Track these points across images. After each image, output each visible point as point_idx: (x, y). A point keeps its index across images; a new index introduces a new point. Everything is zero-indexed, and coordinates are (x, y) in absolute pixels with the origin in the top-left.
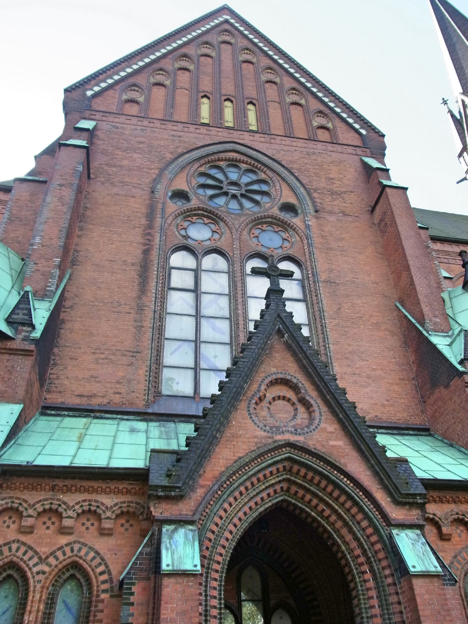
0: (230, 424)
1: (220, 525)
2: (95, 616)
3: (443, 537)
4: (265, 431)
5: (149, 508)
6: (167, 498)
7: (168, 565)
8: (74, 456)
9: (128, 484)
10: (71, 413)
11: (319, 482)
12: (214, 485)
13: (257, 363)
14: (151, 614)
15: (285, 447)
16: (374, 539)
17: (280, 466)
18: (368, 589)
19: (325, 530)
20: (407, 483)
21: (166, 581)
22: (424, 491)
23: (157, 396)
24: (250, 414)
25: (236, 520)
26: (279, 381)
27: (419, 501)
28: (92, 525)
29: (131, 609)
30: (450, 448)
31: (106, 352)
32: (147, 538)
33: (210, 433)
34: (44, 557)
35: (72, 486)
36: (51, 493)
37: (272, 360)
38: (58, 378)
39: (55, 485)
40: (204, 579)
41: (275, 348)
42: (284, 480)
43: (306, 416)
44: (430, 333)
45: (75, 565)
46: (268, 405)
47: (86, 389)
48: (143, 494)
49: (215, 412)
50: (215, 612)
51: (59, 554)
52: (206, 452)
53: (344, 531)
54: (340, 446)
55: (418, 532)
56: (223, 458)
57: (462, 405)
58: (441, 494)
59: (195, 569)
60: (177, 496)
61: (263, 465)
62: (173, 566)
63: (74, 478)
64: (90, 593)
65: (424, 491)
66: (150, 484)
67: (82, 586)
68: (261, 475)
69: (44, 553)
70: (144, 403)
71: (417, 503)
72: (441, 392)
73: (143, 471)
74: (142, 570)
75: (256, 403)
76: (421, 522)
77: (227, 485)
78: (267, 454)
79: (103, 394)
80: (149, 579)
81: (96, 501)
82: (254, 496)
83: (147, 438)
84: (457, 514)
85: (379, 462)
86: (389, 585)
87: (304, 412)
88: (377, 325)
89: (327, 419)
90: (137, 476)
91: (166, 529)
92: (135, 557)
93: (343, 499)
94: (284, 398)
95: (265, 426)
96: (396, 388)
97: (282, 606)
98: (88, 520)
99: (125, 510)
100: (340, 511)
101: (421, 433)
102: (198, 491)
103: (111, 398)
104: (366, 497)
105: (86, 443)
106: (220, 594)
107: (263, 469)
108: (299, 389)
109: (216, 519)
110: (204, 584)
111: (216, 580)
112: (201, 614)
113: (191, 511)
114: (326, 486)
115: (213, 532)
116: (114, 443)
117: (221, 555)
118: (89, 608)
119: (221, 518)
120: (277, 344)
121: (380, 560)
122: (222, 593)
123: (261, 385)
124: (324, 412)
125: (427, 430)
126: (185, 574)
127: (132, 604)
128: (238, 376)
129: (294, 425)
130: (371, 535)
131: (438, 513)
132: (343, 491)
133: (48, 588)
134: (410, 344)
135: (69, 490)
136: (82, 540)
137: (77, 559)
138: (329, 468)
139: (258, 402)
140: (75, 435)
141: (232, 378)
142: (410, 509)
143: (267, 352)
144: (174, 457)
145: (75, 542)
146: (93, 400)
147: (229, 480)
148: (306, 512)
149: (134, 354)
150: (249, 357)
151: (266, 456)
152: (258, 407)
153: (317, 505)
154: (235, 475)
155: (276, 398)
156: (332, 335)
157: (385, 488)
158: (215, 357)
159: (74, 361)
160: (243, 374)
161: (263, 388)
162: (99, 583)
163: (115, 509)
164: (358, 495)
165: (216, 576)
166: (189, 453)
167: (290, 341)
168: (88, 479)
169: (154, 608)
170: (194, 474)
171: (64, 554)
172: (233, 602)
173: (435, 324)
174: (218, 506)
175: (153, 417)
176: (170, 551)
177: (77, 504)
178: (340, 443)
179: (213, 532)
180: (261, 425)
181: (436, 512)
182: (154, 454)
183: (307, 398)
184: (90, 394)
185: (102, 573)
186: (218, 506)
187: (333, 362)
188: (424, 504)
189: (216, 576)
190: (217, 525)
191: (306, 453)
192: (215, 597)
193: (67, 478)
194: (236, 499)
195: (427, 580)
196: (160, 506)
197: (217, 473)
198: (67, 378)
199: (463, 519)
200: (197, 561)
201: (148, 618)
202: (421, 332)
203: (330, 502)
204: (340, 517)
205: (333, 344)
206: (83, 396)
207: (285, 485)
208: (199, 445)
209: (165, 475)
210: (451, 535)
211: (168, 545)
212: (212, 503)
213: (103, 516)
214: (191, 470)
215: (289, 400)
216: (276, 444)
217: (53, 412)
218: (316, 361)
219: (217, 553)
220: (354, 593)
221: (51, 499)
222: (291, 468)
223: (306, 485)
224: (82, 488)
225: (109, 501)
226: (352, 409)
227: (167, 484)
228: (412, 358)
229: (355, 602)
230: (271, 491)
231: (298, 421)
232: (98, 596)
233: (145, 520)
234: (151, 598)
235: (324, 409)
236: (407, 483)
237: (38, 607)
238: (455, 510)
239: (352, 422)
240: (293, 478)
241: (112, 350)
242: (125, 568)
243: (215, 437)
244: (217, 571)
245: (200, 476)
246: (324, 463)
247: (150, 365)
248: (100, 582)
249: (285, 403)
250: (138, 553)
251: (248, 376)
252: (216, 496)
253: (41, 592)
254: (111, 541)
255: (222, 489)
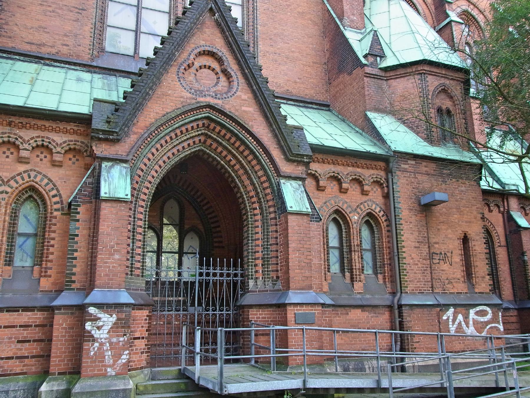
0: (161, 84)
1: (148, 165)
2: (50, 228)
3: (319, 188)
4: (190, 93)
5: (91, 147)
6: (106, 140)
7: (106, 193)
8: (28, 97)
9: (75, 126)
10: (22, 58)
11: (230, 138)
12: (145, 133)
13: (189, 35)
14: (92, 228)
15: (205, 108)
16: (266, 185)
17: (200, 123)
18: (256, 221)
19: (230, 175)
20: (299, 146)
21: (104, 205)
22: (311, 153)
23: (101, 52)
24: (179, 78)
25: (161, 162)
26: (207, 53)
27: (306, 160)
28: (45, 157)
29: (77, 224)
30: (342, 122)
31: (54, 6)
32: (90, 171)
33: (143, 90)
34: (6, 180)
35: (26, 123)
36: (8, 128)
37: (202, 35)
38: (7, 24)
39: (11, 121)
40: (133, 205)
41: (206, 24)
42: (202, 134)
43: (226, 84)
44: (346, 28)
45: (32, 188)
46: (195, 72)
47: (35, 38)
48: (87, 135)
49: (149, 73)
50: (140, 230)
51: (18, 178)
52: (140, 105)
53: (244, 178)
54: (250, 112)
55: (300, 183)
56: (154, 112)
57: (358, 90)
58: (324, 157)
59: (126, 197)
60: (114, 139)
61: (187, 121)
62: (110, 194)
63: (27, 117)
64: (45, 211)
65: (311, 153)
66: (92, 127)
67: (38, 205)
68: (184, 129)
69: (6, 177)
70: (89, 56)
71: (304, 162)
72: (345, 78)
73: (87, 116)
74: (85, 195)
75: (185, 69)
76: (304, 176)
77: (156, 134)
78: (190, 112)
79: (52, 45)
80: (91, 202)
81: (48, 138)
82: (177, 145)
83: (92, 88)
84: (334, 172)
85: (280, 128)
86: (271, 219)
87: (224, 81)
88: (302, 14)
89: (242, 89)
90: (83, 121)
91: (104, 164)
92: (80, 185)
93: (246, 153)
94: (209, 67)
95: (191, 89)
96: (309, 69)
97: (193, 229)
98: (42, 153)
99: (72, 147)
100: (243, 162)
101: (322, 108)
102: (132, 136)
103: (60, 49)
104: (265, 153)
105: (37, 87)
106: (146, 217)
107: (186, 124)
108: (223, 62)
109: (146, 160)
110: (133, 209)
111: (142, 207)
112: (129, 231)
113: (125, 152)
114: (235, 142)
115: (142, 170)
116: (62, 89)
117: (148, 188)
118: (45, 221)
119: (149, 160)
120: (208, 20)
121: (268, 201)
122: (147, 216)
123: (191, 54)
124: (241, 83)
125: (328, 106)
126: (118, 201)
127: (78, 221)
128: (171, 44)
129: (215, 91)
130: (264, 182)
131: (319, 171)
132: (247, 147)
133: (11, 205)
134: (328, 34)
135: (23, 126)
136: (37, 169)
137: (35, 184)
138: (239, 128)
139: (187, 68)
140: (27, 78)
141: (165, 46)
142: (297, 165)
143: (199, 26)
144: (113, 107)
145: (31, 170)
146: (43, 48)
147: (157, 130)
148: (217, 161)
149: (80, 11)
150: (182, 29)
151: (189, 114)
152: (187, 73)
153: (226, 156)
154: (162, 126)
155: (203, 67)
156: (261, 18)
157: (281, 148)
158: (155, 23)
159: (22, 9)
160: (176, 43)
161: (192, 57)
162: (53, 204)
163: (64, 145)
164: (258, 152)
165: (143, 204)
166: (125, 105)
167: (219, 20)
168: (40, 119)
169: (94, 224)
170: (128, 123)
171: (23, 179)
172: (156, 225)
173: (352, 21)
174: (147, 150)
175: (97, 70)
176: (107, 183)
177: (32, 139)
178: (251, 109)
179: (142, 170)
180: (188, 88)
181: (318, 170)
182: (96, 102)
183: (229, 70)
184: (39, 42)
185: (54, 196)
186: (147, 150)
187: (258, 40)
188: (309, 163)
189: (143, 204)
190: (146, 165)
191: (222, 115)
192: (141, 220)
193: (22, 116)
194: (162, 146)
195: (299, 217)
196: (101, 146)
197: (148, 124)
198: (16, 25)
199: (317, 177)
200: (128, 191)
201: (90, 232)
202: (338, 26)
203: (237, 154)
204: (242, 167)
205: (260, 25)
206: (33, 44)
207: (202, 138)
208: (134, 99)
209: (105, 121)
210: (325, 187)
211: (106, 178)
212: (142, 147)
213: (54, 151)
214: (127, 119)
215: (213, 70)
216: (199, 105)
217: (4, 55)
218: (240, 40)
219: (145, 187)
220: (245, 223)
221: (9, 133)
222: (209, 125)
223: (220, 140)
224: (36, 126)
225: (59, 139)
226: (265, 83)
227: (107, 129)
228: (327, 47)
229: (245, 229)
230: (191, 142)
231: (219, 88)
232: (51, 213)
233: (88, 156)
234: (93, 216)
235: (242, 80)
236: (299, 146)
237: (5, 218)
238: (333, 169)
239: (263, 94)
240: (209, 133)
241: (59, 4)
242: (72, 193)
243: (148, 94)
244: (144, 200)
245: (134, 124)
246: (236, 124)
247: (95, 23)
248: (52, 202)
249: (210, 71)
250: (82, 182)
251: (180, 45)
252: (146, 142)
253: (6, 207)
254: (61, 171)
255: (151, 136)
